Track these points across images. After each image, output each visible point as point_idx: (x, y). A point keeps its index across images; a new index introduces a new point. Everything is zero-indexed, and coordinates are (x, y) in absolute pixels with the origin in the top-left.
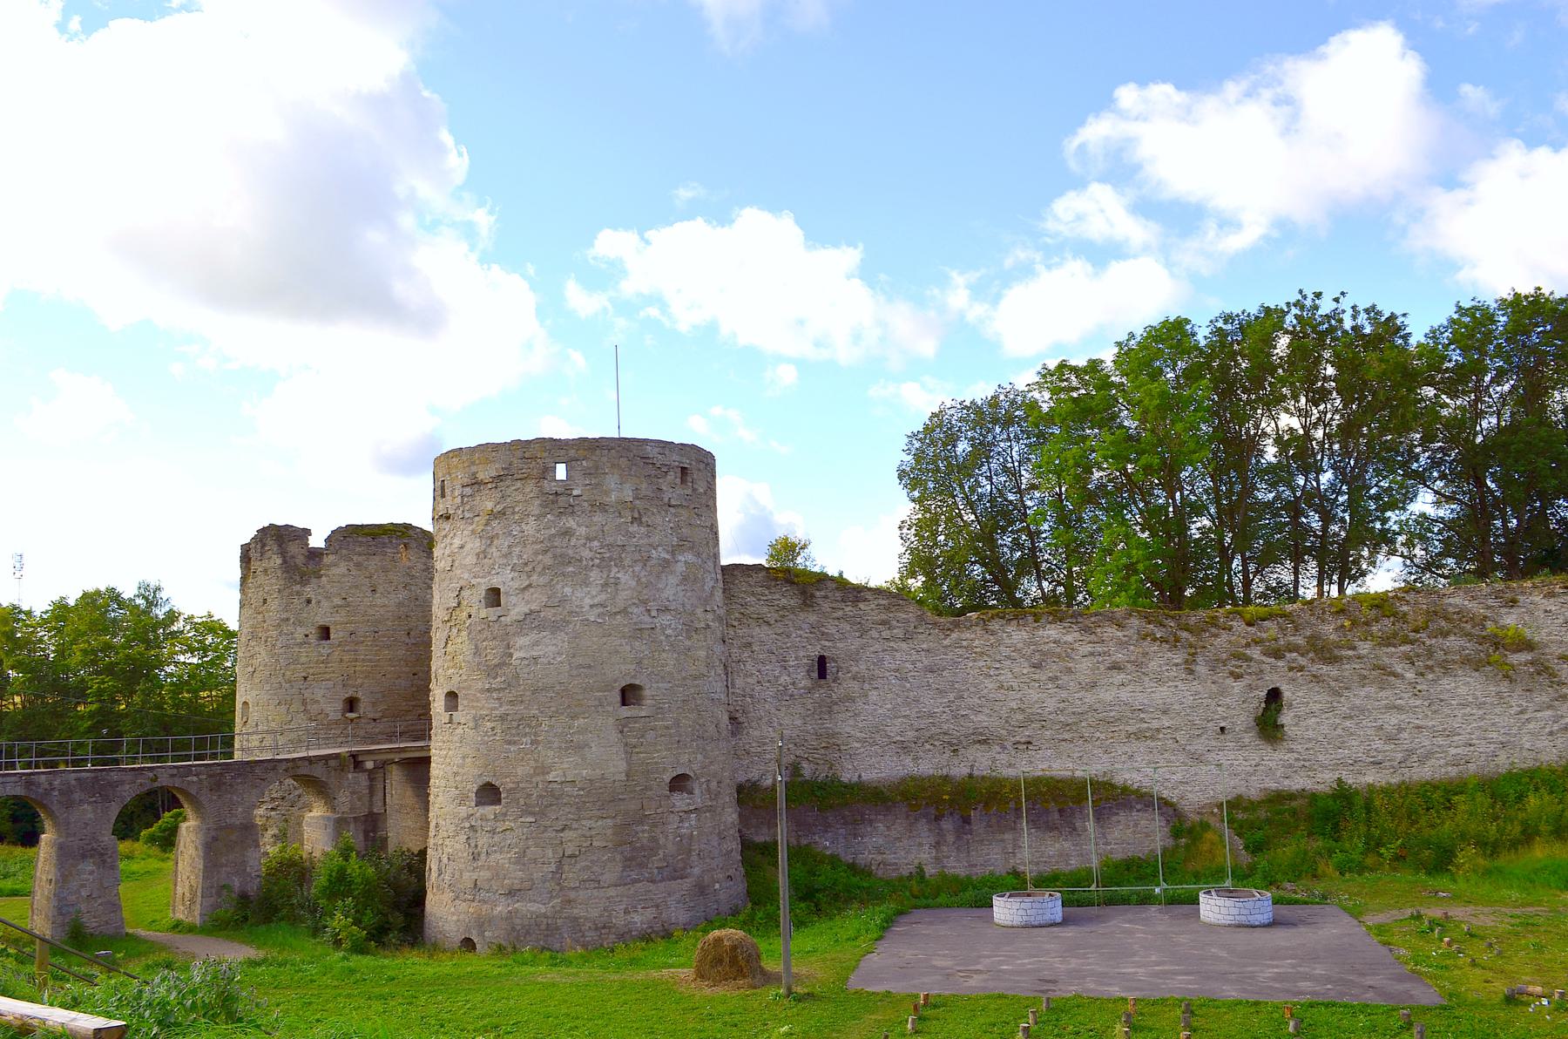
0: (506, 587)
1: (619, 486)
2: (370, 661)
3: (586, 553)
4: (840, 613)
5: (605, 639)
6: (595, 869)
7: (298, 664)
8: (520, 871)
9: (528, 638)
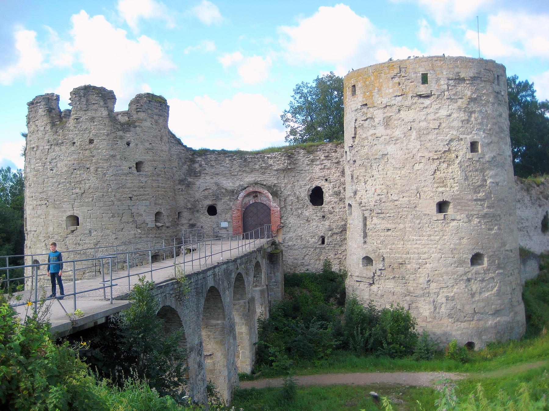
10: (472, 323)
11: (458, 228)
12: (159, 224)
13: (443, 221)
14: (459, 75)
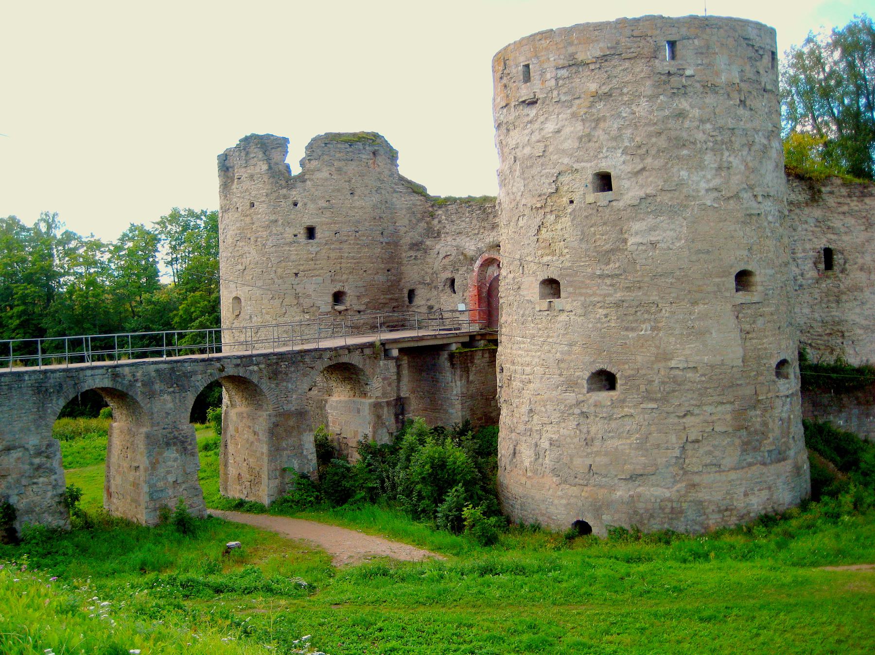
0: (617, 171)
1: (728, 67)
2: (353, 258)
3: (700, 136)
4: (845, 208)
5: (721, 224)
6: (717, 453)
7: (289, 261)
8: (642, 456)
9: (645, 223)
10: (586, 489)
11: (567, 325)
12: (339, 308)
13: (548, 312)
14: (574, 58)
